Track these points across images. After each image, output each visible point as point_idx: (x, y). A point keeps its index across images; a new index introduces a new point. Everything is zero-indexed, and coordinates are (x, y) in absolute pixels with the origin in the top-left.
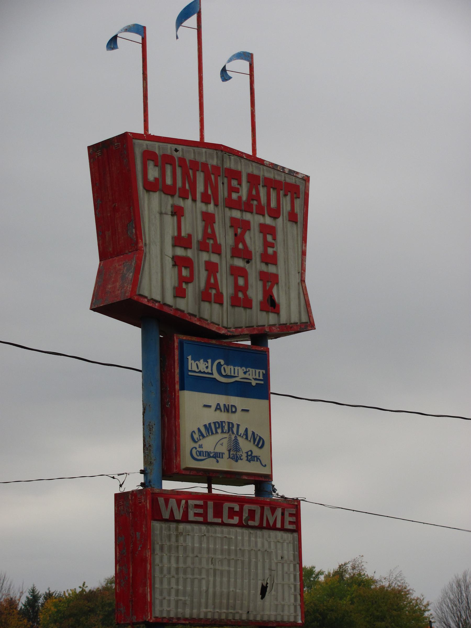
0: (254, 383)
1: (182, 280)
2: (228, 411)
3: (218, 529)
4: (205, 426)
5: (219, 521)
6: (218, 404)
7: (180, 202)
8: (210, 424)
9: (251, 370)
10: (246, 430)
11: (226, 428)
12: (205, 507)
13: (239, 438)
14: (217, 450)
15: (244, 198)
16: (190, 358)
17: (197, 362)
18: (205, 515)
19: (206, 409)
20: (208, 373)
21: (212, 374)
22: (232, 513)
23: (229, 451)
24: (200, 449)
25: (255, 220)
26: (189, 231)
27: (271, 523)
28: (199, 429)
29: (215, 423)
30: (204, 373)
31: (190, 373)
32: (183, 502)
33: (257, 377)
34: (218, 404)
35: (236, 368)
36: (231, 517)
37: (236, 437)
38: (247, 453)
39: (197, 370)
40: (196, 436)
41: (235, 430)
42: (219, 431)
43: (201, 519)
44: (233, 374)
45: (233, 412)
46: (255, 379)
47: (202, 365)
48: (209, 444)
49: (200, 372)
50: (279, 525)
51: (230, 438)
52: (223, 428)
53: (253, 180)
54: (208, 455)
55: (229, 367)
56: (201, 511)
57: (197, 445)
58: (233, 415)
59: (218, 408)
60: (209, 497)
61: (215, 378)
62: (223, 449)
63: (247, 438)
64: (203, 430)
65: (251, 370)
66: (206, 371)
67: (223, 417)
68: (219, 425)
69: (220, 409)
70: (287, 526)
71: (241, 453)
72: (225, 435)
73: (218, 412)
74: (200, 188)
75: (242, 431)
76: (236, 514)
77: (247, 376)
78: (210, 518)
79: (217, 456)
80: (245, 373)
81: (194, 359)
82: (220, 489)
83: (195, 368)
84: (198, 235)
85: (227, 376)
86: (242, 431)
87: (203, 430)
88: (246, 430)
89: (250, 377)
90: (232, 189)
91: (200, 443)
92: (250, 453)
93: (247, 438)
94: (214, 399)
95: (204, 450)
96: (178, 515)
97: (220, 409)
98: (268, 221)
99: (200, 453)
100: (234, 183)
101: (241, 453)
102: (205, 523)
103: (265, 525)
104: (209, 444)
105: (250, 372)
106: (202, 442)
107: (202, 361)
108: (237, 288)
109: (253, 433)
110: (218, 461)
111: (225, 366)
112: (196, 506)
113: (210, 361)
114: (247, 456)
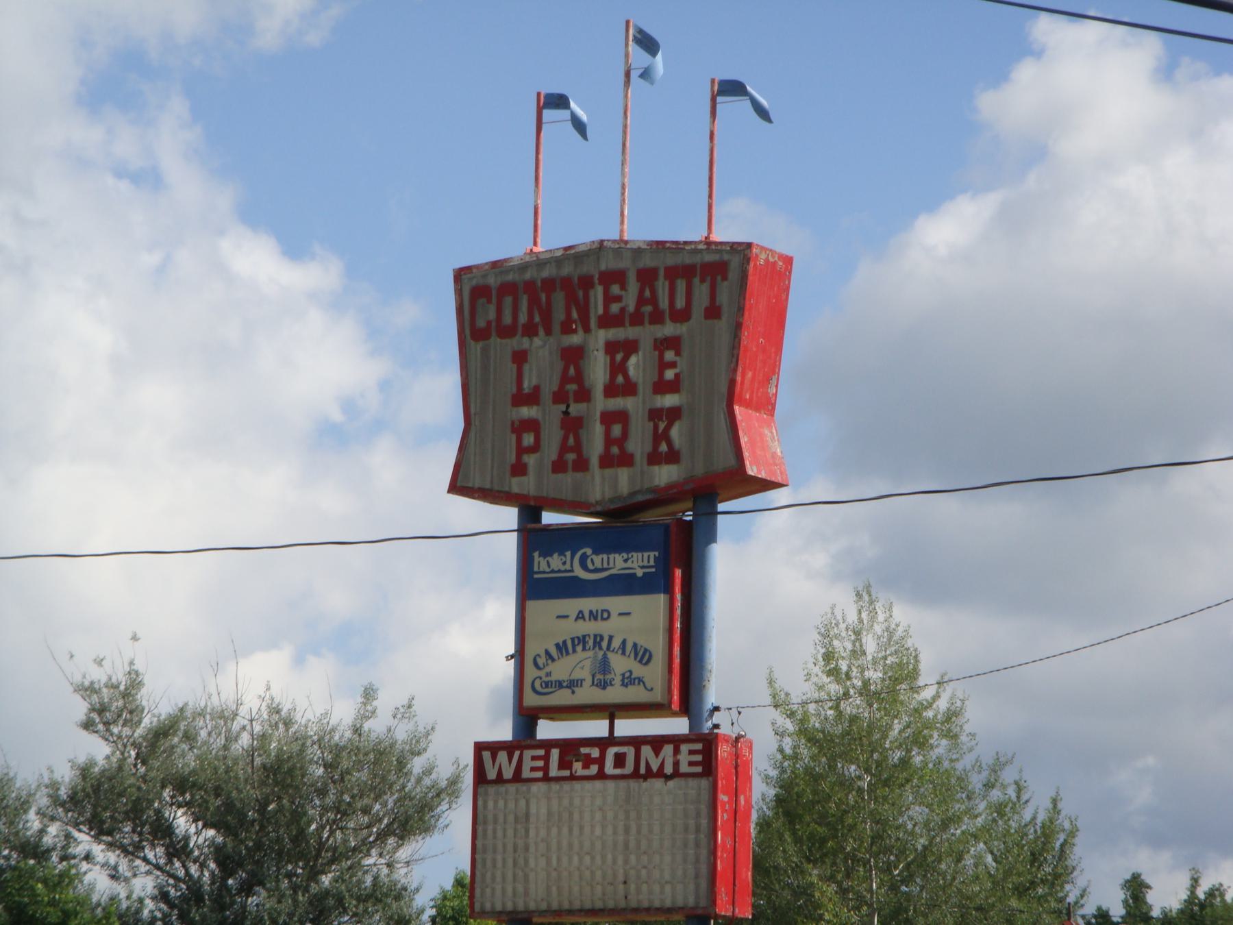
0: (640, 573)
1: (521, 450)
2: (596, 619)
3: (566, 786)
4: (557, 645)
5: (566, 773)
6: (581, 612)
7: (525, 343)
8: (564, 642)
9: (635, 554)
10: (624, 642)
11: (591, 642)
12: (546, 758)
13: (610, 655)
14: (576, 676)
15: (631, 308)
16: (536, 554)
17: (549, 559)
18: (546, 769)
19: (563, 621)
20: (566, 571)
21: (572, 571)
22: (587, 762)
23: (593, 676)
24: (546, 679)
25: (646, 334)
26: (534, 382)
27: (655, 768)
28: (547, 652)
29: (573, 639)
30: (559, 571)
31: (536, 576)
32: (517, 753)
33: (646, 563)
34: (581, 612)
35: (612, 556)
36: (586, 766)
37: (605, 654)
38: (623, 675)
39: (548, 570)
40: (541, 662)
41: (604, 645)
42: (579, 648)
43: (540, 774)
44: (605, 566)
45: (603, 619)
46: (643, 567)
47: (556, 562)
48: (561, 670)
49: (553, 571)
50: (669, 770)
51: (595, 656)
52: (585, 643)
53: (647, 277)
54: (560, 685)
55: (600, 556)
56: (540, 763)
57: (542, 673)
58: (605, 623)
59: (580, 616)
60: (611, 740)
61: (576, 577)
62: (584, 673)
63: (624, 653)
64: (554, 652)
65: (636, 556)
66: (563, 568)
67: (589, 628)
68: (582, 640)
69: (583, 618)
70: (684, 768)
71: (612, 676)
72: (590, 654)
73: (580, 622)
74: (559, 315)
75: (616, 643)
76: (594, 761)
77: (629, 564)
78: (554, 772)
79: (573, 684)
80: (626, 561)
81: (542, 555)
82: (627, 727)
83: (544, 567)
84: (550, 385)
85: (596, 570)
86: (616, 643)
87: (554, 652)
88: (624, 642)
89: (635, 565)
90: (609, 299)
91: (548, 669)
92: (627, 675)
93: (624, 653)
94: (572, 606)
95: (554, 678)
96: (508, 773)
97: (583, 618)
98: (669, 329)
99: (547, 684)
100: (615, 289)
101: (612, 676)
102: (546, 778)
103: (643, 770)
104: (561, 670)
105: (635, 558)
106: (552, 667)
107: (556, 555)
108: (609, 441)
109: (635, 645)
110: (573, 692)
111: (594, 557)
112: (534, 758)
113: (568, 554)
114: (623, 680)
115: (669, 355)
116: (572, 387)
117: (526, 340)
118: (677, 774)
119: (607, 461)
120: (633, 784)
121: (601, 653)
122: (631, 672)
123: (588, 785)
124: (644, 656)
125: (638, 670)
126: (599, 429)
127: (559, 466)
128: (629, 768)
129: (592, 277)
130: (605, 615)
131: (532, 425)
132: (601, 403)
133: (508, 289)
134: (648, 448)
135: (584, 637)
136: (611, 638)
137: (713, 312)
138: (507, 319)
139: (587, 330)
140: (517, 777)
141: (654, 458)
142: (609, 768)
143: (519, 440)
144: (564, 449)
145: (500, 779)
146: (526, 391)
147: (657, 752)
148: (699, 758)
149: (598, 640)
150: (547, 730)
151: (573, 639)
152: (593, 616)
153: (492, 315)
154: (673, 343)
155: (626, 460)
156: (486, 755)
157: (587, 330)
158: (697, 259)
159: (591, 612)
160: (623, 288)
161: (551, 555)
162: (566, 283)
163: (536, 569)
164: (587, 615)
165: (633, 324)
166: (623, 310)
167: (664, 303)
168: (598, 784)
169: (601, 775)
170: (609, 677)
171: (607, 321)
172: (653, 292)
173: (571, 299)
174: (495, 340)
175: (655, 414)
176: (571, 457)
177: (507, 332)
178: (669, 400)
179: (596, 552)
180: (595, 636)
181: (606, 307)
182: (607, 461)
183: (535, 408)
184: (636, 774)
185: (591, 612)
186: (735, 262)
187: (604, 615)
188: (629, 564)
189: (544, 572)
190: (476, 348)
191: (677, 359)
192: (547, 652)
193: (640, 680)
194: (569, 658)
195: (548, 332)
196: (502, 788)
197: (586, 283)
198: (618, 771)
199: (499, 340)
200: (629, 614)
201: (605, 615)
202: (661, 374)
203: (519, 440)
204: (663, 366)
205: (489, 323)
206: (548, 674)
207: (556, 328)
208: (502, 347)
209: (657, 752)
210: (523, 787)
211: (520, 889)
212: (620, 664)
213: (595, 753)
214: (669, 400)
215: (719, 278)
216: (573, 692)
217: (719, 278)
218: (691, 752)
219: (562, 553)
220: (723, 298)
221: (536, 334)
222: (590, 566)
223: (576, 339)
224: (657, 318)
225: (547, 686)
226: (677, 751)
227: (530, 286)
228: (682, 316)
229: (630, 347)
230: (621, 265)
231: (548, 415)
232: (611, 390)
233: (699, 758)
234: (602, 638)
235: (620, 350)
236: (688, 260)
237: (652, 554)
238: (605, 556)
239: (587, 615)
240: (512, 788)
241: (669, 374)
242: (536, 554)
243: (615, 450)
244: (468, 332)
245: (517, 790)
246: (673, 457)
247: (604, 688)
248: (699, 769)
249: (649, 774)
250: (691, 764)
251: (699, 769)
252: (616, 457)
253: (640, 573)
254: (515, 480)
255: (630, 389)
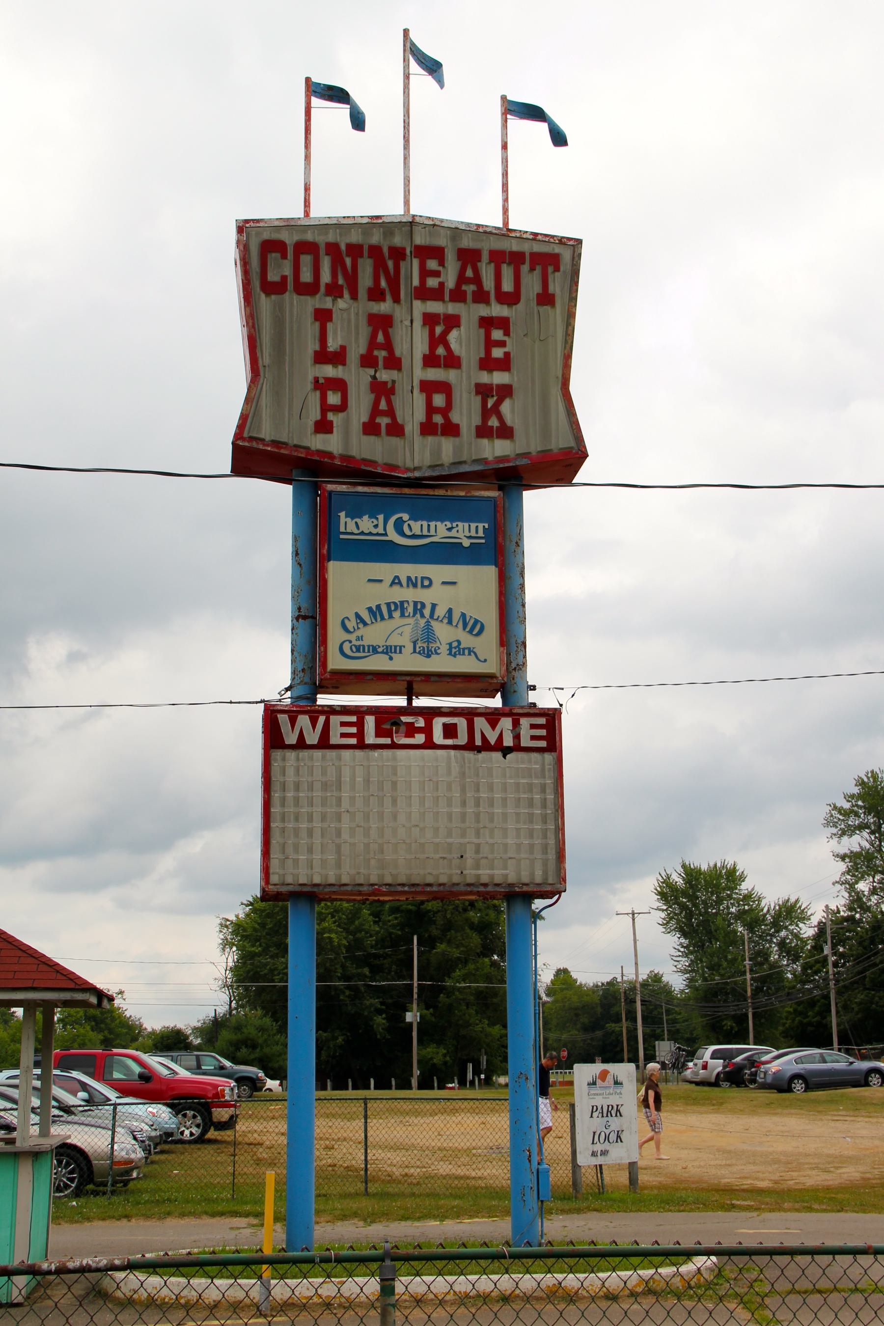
0: (466, 543)
1: (325, 408)
2: (415, 586)
10: (450, 611)
11: (410, 609)
12: (360, 724)
13: (433, 623)
14: (395, 641)
16: (342, 514)
17: (358, 520)
18: (360, 735)
20: (378, 534)
21: (386, 535)
22: (411, 730)
23: (415, 643)
24: (358, 643)
25: (470, 313)
26: (340, 342)
29: (388, 605)
30: (370, 534)
31: (342, 536)
32: (322, 719)
33: (473, 534)
35: (433, 524)
38: (450, 644)
39: (356, 531)
40: (350, 625)
41: (427, 612)
42: (396, 614)
44: (425, 533)
45: (423, 586)
46: (470, 537)
47: (366, 524)
48: (374, 634)
49: (362, 533)
50: (508, 741)
53: (469, 257)
54: (375, 650)
55: (419, 523)
57: (352, 637)
58: (426, 591)
62: (404, 638)
63: (450, 622)
64: (366, 616)
66: (374, 531)
67: (409, 595)
68: (401, 606)
70: (525, 742)
71: (438, 644)
72: (411, 621)
73: (396, 588)
74: (365, 280)
75: (440, 612)
76: (420, 730)
77: (453, 533)
79: (390, 651)
80: (449, 529)
83: (351, 527)
84: (357, 348)
85: (414, 537)
86: (440, 612)
87: (366, 616)
90: (425, 273)
91: (359, 633)
92: (455, 644)
93: (450, 622)
94: (386, 570)
95: (366, 642)
96: (312, 738)
97: (400, 584)
98: (497, 310)
100: (432, 264)
101: (438, 644)
102: (362, 745)
103: (478, 742)
104: (374, 634)
107: (366, 517)
108: (431, 409)
109: (463, 615)
111: (412, 523)
113: (381, 517)
114: (450, 649)
115: (497, 334)
116: (381, 351)
117: (329, 299)
118: (517, 748)
119: (427, 429)
120: (469, 755)
121: (422, 622)
122: (459, 642)
123: (346, 754)
124: (476, 628)
125: (467, 640)
126: (419, 400)
127: (371, 428)
128: (462, 738)
129: (404, 249)
130: (426, 583)
131: (340, 385)
132: (420, 373)
133: (305, 247)
134: (477, 420)
135: (402, 603)
136: (434, 606)
137: (546, 299)
138: (306, 276)
139: (396, 299)
140: (324, 743)
141: (483, 432)
142: (438, 736)
143: (324, 398)
144: (375, 411)
145: (301, 744)
146: (331, 349)
147: (493, 724)
148: (543, 732)
149: (419, 607)
150: (323, 700)
151: (388, 605)
152: (412, 583)
153: (288, 271)
154: (504, 324)
155: (451, 430)
156: (283, 719)
157: (396, 299)
158: (526, 248)
159: (409, 578)
160: (442, 263)
161: (360, 517)
162: (375, 251)
163: (342, 529)
164: (404, 582)
165: (452, 299)
166: (442, 285)
167: (488, 284)
168: (358, 753)
169: (429, 744)
170: (433, 646)
171: (423, 293)
172: (476, 271)
173: (379, 265)
174: (290, 299)
175: (483, 390)
176: (384, 421)
177: (310, 289)
178: (499, 378)
179: (414, 518)
180: (415, 603)
181: (423, 281)
182: (427, 429)
183: (340, 367)
184: (470, 746)
185: (409, 578)
186: (566, 255)
187: (427, 583)
188: (453, 533)
189: (352, 534)
190: (265, 303)
191: (506, 338)
192: (357, 616)
193: (471, 651)
194: (383, 623)
195: (354, 296)
196: (304, 754)
197: (398, 254)
198: (449, 742)
199: (295, 296)
200: (454, 583)
201: (426, 583)
202: (488, 352)
203: (324, 398)
204: (490, 344)
205: (284, 278)
206: (358, 639)
207: (362, 293)
208: (300, 308)
209: (493, 724)
210: (331, 754)
211: (331, 857)
212: (444, 633)
213: (421, 723)
214: (499, 378)
215: (550, 269)
216: (391, 658)
217: (550, 269)
218: (533, 726)
219: (373, 516)
220: (556, 286)
221: (341, 296)
222: (408, 532)
223: (384, 307)
224: (481, 297)
225: (358, 650)
226: (516, 724)
227: (333, 249)
228: (512, 299)
229: (453, 322)
230: (441, 242)
231: (358, 379)
232: (430, 361)
233: (543, 732)
234: (423, 605)
235: (439, 327)
236: (515, 247)
237: (481, 526)
238: (425, 523)
239: (404, 582)
240: (318, 754)
241: (497, 353)
242: (342, 514)
243: (438, 419)
244: (256, 283)
245: (324, 757)
246: (506, 432)
247: (429, 656)
248: (543, 744)
249: (486, 746)
250: (533, 738)
251: (543, 744)
252: (437, 424)
253: (466, 543)
254: (320, 437)
255: (452, 361)
